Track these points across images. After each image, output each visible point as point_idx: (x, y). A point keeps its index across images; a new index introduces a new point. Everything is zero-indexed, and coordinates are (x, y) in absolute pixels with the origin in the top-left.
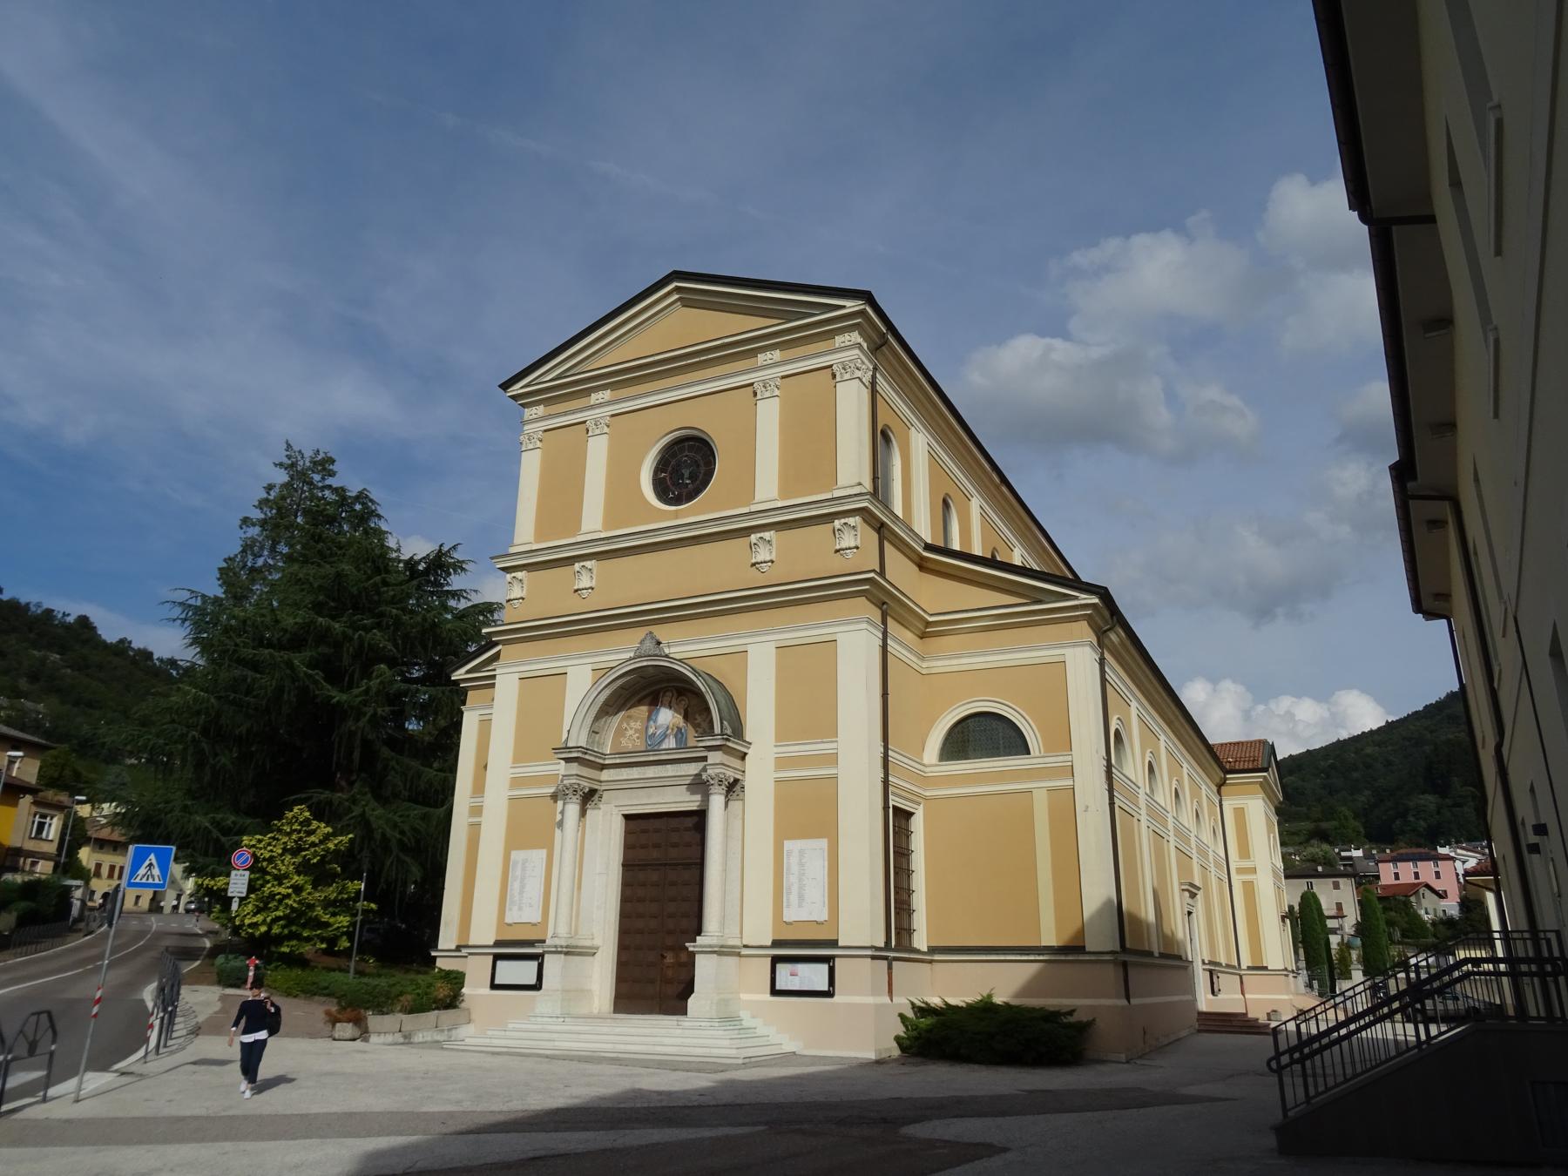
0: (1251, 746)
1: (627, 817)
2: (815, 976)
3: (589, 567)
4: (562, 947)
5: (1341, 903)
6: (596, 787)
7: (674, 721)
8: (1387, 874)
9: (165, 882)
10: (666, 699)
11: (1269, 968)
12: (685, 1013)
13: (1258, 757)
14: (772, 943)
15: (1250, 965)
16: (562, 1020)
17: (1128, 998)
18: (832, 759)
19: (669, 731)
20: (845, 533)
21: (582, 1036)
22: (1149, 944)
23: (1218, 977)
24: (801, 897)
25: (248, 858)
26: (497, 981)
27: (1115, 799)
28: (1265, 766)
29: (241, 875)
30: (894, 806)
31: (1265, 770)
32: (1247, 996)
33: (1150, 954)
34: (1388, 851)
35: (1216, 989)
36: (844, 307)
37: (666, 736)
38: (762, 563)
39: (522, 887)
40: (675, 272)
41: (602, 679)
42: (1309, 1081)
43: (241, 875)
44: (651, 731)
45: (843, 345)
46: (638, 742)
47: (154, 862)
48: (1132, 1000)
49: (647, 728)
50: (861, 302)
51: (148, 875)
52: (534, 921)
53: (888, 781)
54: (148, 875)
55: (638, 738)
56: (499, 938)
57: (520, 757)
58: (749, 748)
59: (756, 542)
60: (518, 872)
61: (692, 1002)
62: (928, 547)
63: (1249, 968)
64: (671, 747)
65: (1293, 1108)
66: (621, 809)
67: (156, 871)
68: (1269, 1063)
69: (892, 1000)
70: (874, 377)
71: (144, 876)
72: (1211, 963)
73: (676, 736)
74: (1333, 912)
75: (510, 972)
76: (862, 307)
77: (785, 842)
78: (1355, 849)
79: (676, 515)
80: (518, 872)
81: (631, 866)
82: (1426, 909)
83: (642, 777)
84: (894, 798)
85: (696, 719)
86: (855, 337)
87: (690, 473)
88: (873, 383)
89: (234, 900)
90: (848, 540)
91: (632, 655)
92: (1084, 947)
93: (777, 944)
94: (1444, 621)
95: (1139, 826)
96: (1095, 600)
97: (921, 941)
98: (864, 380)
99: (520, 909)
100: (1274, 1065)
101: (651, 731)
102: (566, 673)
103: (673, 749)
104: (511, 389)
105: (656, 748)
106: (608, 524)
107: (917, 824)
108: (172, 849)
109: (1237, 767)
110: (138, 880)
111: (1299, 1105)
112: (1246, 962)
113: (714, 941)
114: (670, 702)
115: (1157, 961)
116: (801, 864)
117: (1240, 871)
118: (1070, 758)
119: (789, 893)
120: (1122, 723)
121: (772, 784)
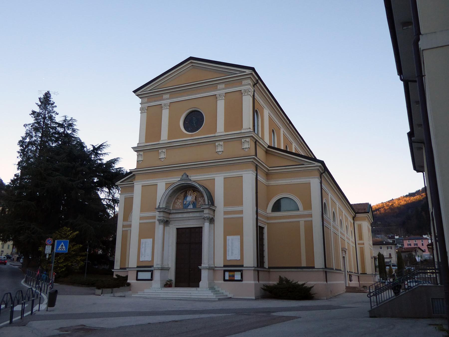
0: (364, 205)
3: (164, 151)
4: (160, 268)
5: (391, 254)
6: (168, 220)
7: (192, 200)
8: (406, 244)
10: (190, 193)
11: (367, 274)
12: (199, 287)
13: (366, 208)
14: (224, 266)
15: (361, 273)
16: (161, 289)
17: (327, 281)
18: (241, 212)
19: (191, 203)
21: (168, 294)
22: (333, 266)
23: (352, 276)
24: (232, 253)
27: (324, 224)
28: (368, 211)
29: (49, 247)
30: (259, 226)
31: (368, 213)
32: (360, 282)
33: (333, 269)
34: (407, 237)
35: (351, 280)
36: (246, 72)
37: (189, 205)
38: (219, 152)
39: (145, 250)
40: (191, 57)
41: (170, 187)
43: (49, 247)
44: (185, 203)
45: (245, 84)
48: (328, 282)
50: (251, 71)
51: (62, 248)
53: (258, 218)
56: (138, 265)
57: (142, 211)
58: (216, 208)
59: (217, 145)
60: (144, 246)
61: (201, 283)
62: (269, 147)
63: (361, 274)
64: (191, 208)
65: (373, 306)
67: (64, 247)
68: (368, 296)
69: (259, 282)
70: (254, 93)
71: (60, 249)
72: (350, 272)
73: (193, 204)
74: (388, 257)
75: (142, 275)
76: (251, 72)
77: (227, 236)
78: (396, 236)
79: (192, 136)
80: (144, 246)
81: (179, 243)
82: (418, 255)
84: (260, 223)
85: (199, 199)
86: (249, 81)
88: (254, 96)
89: (47, 255)
90: (246, 146)
91: (179, 179)
92: (315, 267)
93: (138, 267)
94: (422, 173)
95: (330, 231)
96: (320, 164)
97: (266, 265)
98: (251, 95)
99: (145, 257)
100: (369, 296)
101: (185, 203)
102: (157, 184)
103: (191, 208)
104: (136, 93)
105: (186, 208)
106: (169, 138)
107: (265, 231)
109: (359, 212)
110: (59, 250)
111: (375, 305)
112: (360, 272)
113: (207, 265)
114: (191, 194)
115: (335, 271)
116: (232, 243)
117: (359, 244)
119: (228, 252)
120: (326, 200)
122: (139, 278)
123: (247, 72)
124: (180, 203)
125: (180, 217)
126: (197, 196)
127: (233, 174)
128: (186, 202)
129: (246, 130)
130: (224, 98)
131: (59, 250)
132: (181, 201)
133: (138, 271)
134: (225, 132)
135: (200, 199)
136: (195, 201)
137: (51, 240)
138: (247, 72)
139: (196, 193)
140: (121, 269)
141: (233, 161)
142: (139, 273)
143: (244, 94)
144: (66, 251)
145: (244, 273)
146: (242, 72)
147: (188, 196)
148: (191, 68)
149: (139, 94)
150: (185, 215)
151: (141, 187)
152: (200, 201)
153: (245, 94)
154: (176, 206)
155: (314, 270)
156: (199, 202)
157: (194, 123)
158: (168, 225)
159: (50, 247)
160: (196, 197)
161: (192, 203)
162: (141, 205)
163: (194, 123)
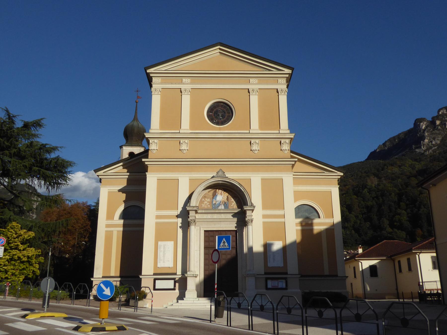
1: (205, 231)
2: (282, 284)
7: (223, 200)
9: (230, 247)
18: (284, 216)
19: (221, 203)
20: (285, 145)
25: (3, 241)
26: (156, 288)
36: (284, 71)
37: (220, 205)
44: (214, 202)
46: (209, 206)
47: (225, 241)
51: (224, 245)
52: (170, 266)
54: (224, 245)
55: (209, 204)
64: (222, 208)
66: (204, 228)
67: (226, 244)
71: (222, 246)
73: (224, 205)
79: (220, 129)
80: (162, 249)
83: (212, 218)
87: (222, 115)
93: (155, 274)
99: (164, 262)
101: (214, 202)
103: (223, 209)
105: (216, 208)
108: (230, 236)
110: (221, 247)
114: (221, 193)
121: (262, 223)
123: (286, 71)
124: (208, 202)
125: (209, 218)
129: (285, 131)
130: (189, 93)
131: (221, 247)
132: (209, 200)
133: (267, 279)
134: (160, 130)
136: (226, 201)
138: (286, 71)
142: (157, 282)
143: (252, 93)
144: (229, 249)
147: (217, 195)
150: (215, 216)
151: (189, 180)
154: (203, 205)
155: (337, 278)
156: (232, 203)
157: (220, 115)
159: (2, 248)
161: (223, 204)
163: (220, 115)
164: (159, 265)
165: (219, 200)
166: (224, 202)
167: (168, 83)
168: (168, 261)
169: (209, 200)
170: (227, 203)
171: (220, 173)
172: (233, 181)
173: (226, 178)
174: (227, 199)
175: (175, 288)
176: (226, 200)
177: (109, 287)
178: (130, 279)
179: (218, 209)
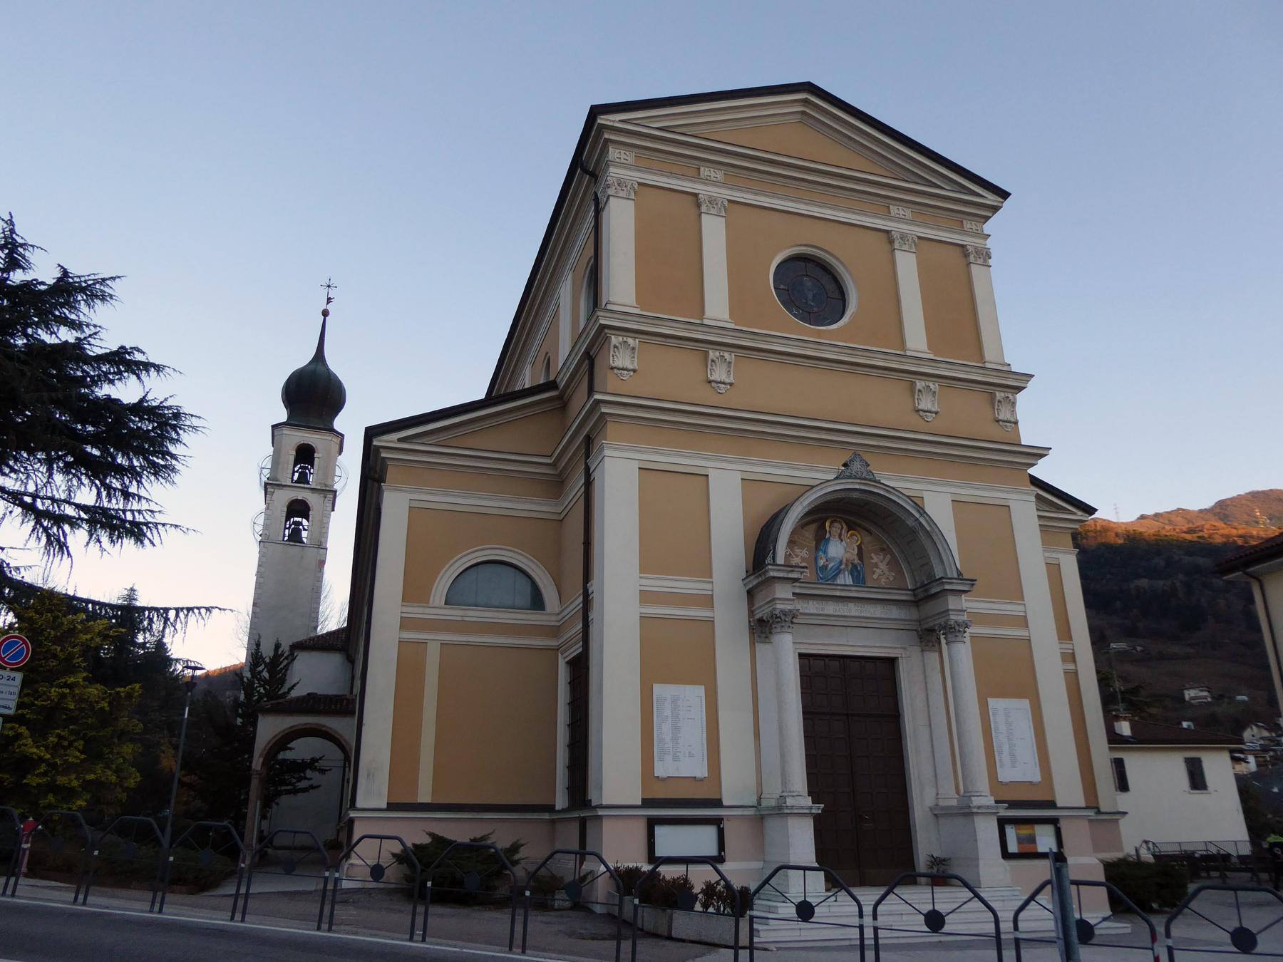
1: (801, 656)
7: (848, 555)
19: (843, 567)
24: (1013, 757)
37: (840, 572)
39: (676, 731)
40: (809, 84)
42: (11, 891)
44: (821, 563)
49: (816, 559)
57: (648, 564)
60: (668, 712)
64: (848, 583)
73: (851, 573)
79: (819, 334)
80: (668, 712)
93: (647, 803)
99: (676, 759)
101: (821, 563)
114: (840, 535)
118: (1070, 646)
119: (1000, 753)
122: (659, 852)
123: (990, 200)
125: (812, 612)
126: (863, 546)
127: (688, 461)
128: (825, 560)
133: (652, 823)
135: (875, 559)
136: (857, 561)
137: (24, 642)
138: (990, 200)
139: (859, 536)
140: (391, 807)
141: (925, 446)
142: (660, 831)
145: (727, 826)
146: (930, 184)
147: (829, 538)
148: (792, 117)
149: (616, 125)
152: (876, 565)
153: (712, 210)
156: (875, 569)
157: (810, 296)
158: (767, 637)
160: (859, 547)
161: (849, 569)
162: (755, 556)
164: (660, 771)
165: (835, 556)
166: (852, 564)
167: (661, 173)
168: (691, 755)
169: (805, 553)
170: (859, 568)
171: (856, 466)
172: (897, 493)
173: (875, 481)
174: (857, 555)
175: (723, 853)
176: (856, 557)
177: (818, 866)
178: (529, 816)
179: (835, 583)
